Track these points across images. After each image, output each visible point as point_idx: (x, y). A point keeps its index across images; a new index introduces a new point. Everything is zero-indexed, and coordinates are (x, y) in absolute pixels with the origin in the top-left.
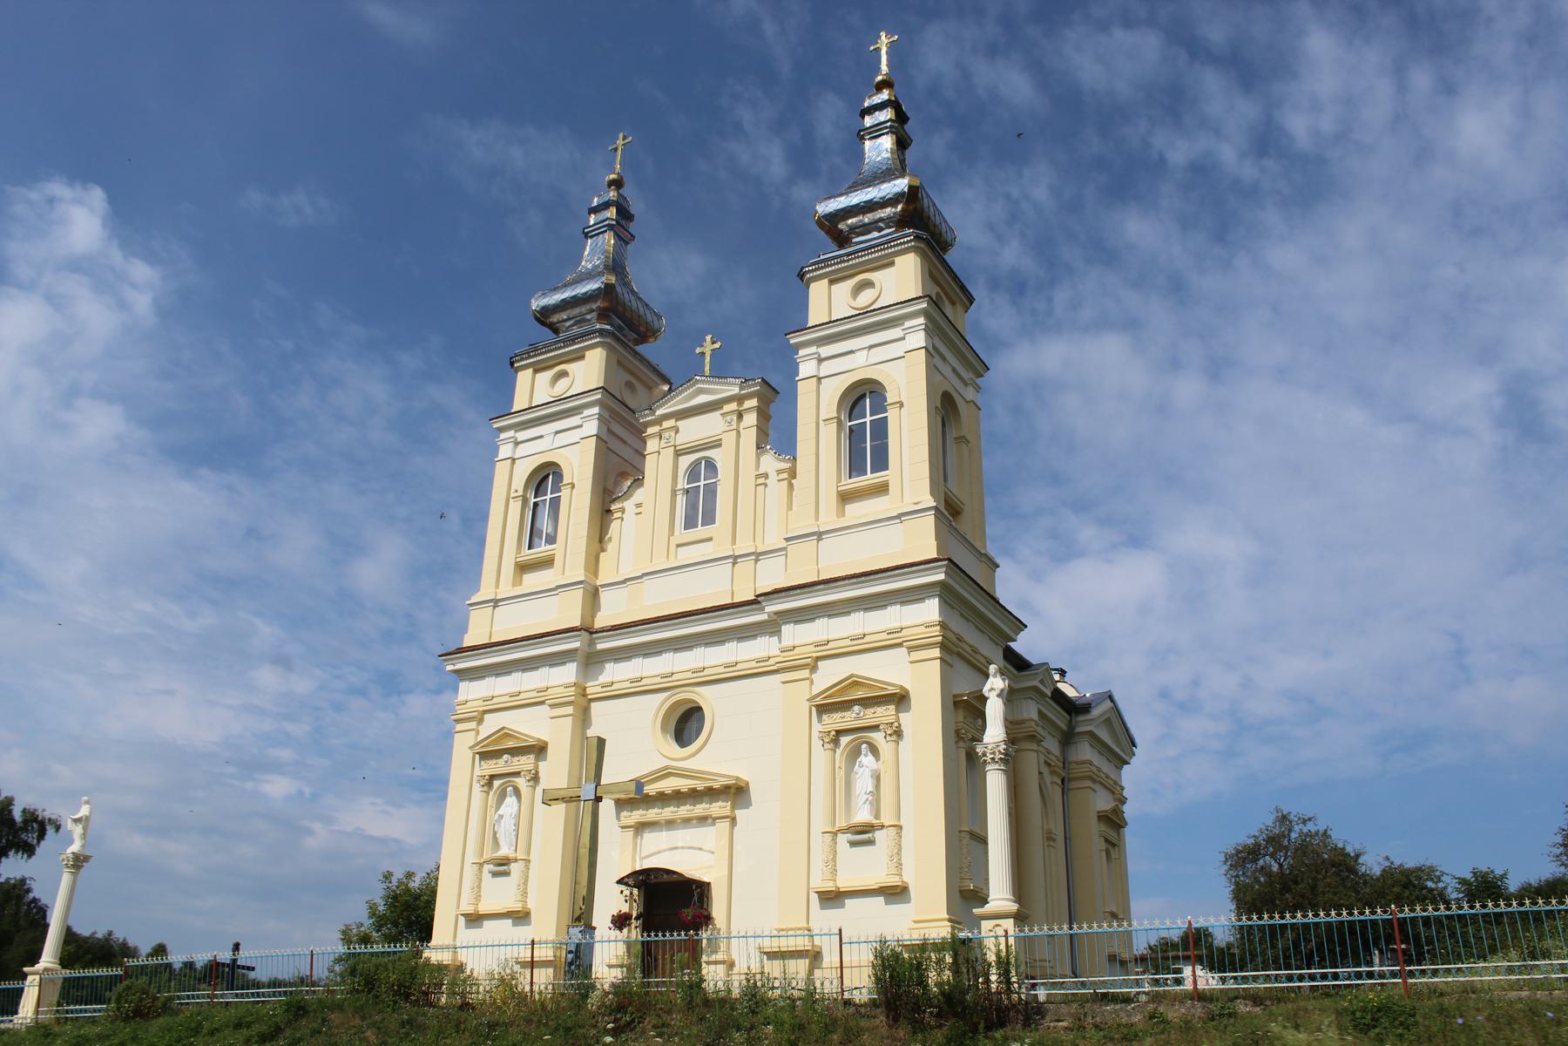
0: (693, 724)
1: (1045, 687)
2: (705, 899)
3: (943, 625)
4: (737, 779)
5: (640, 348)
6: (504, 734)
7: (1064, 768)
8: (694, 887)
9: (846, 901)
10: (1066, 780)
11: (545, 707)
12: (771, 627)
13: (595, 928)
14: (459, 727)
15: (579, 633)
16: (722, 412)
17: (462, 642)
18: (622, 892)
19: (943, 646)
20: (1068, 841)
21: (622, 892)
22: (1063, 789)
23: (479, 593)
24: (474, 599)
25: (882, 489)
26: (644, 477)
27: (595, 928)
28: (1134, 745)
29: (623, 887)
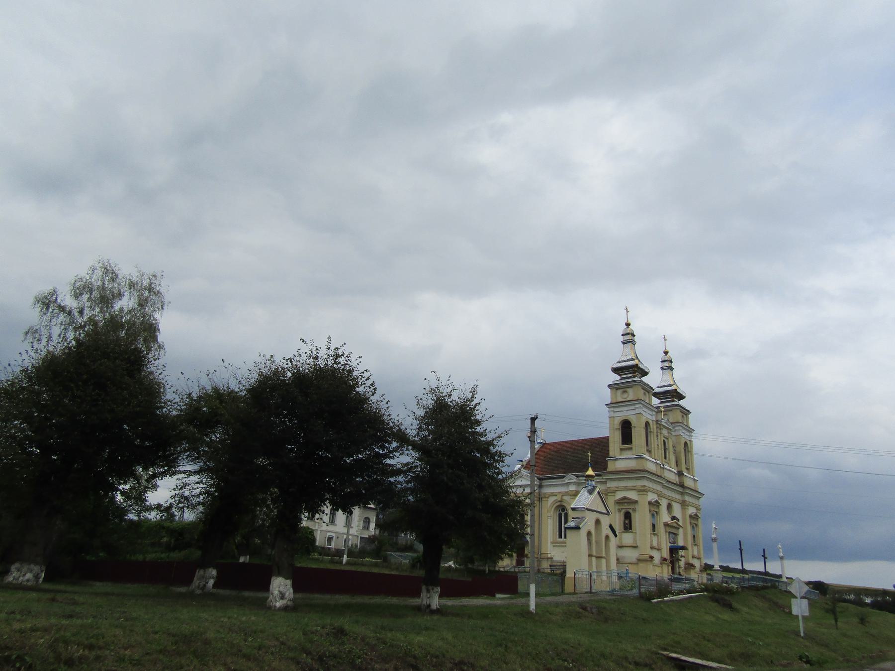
25: (631, 449)
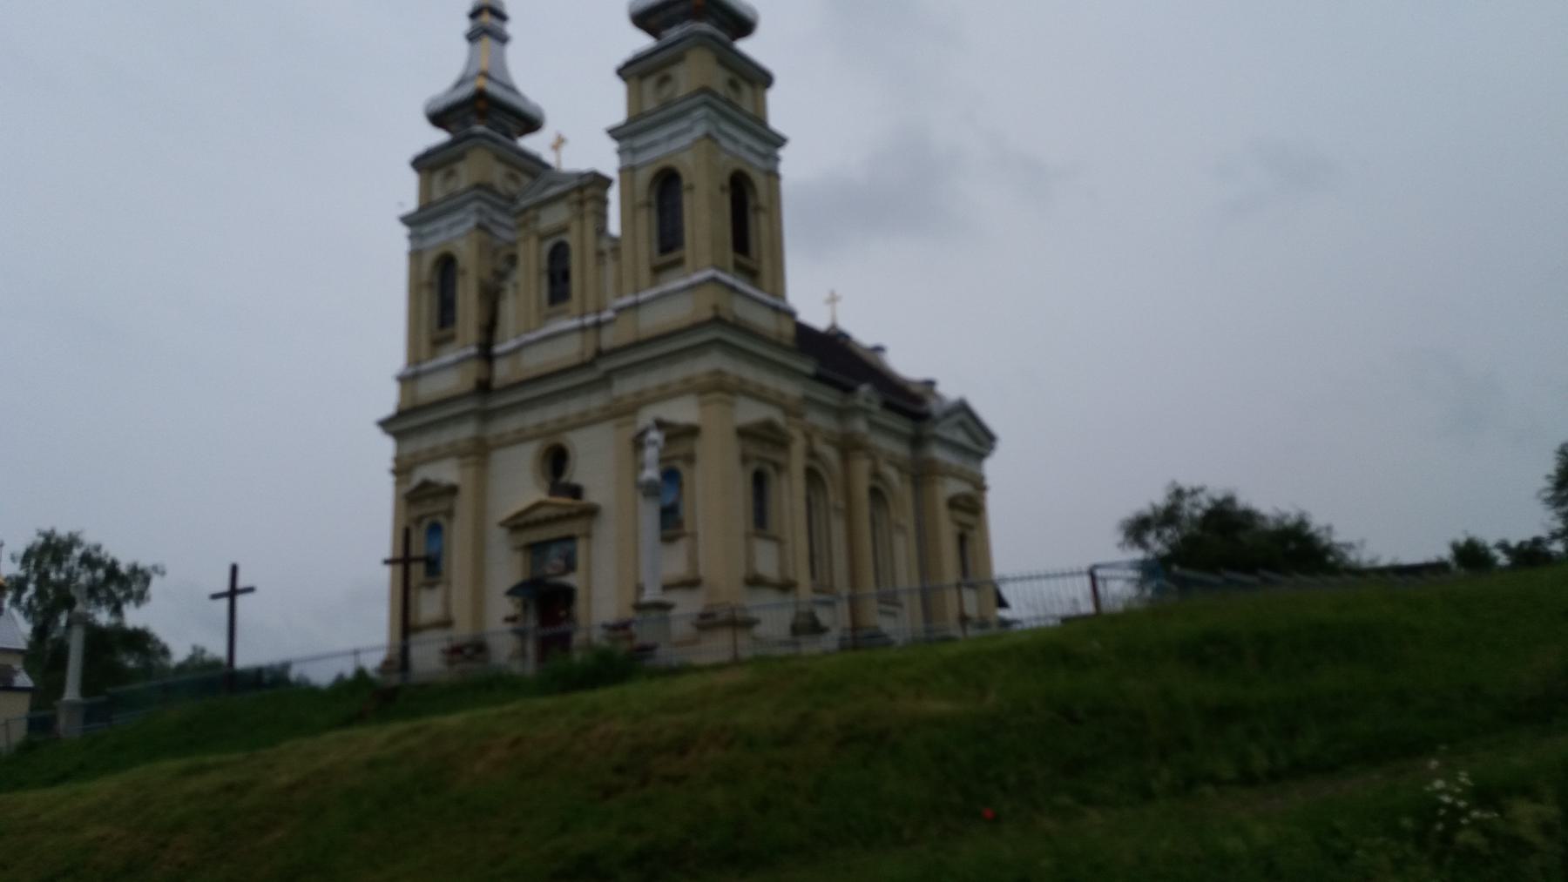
12: (606, 380)
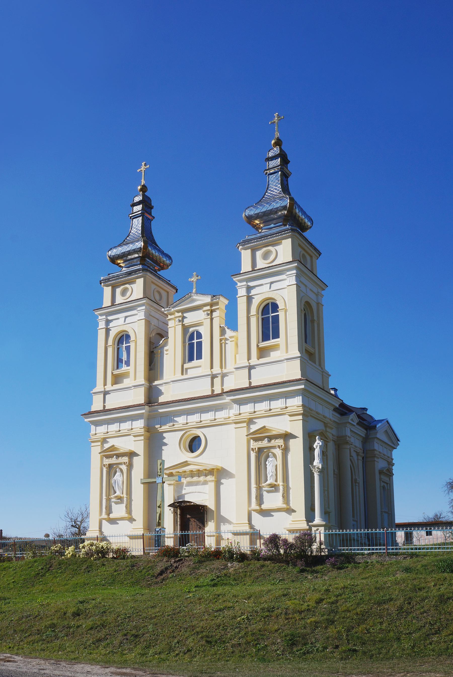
0: (196, 442)
1: (354, 422)
2: (205, 512)
3: (303, 406)
4: (217, 466)
5: (161, 273)
6: (113, 448)
7: (363, 453)
8: (200, 508)
9: (291, 440)
10: (365, 458)
11: (131, 437)
13: (165, 528)
14: (93, 444)
15: (143, 407)
16: (203, 310)
17: (91, 410)
18: (170, 510)
19: (303, 415)
20: (365, 483)
21: (170, 510)
22: (363, 462)
23: (96, 388)
24: (94, 391)
26: (168, 338)
27: (165, 528)
28: (399, 441)
29: (171, 508)
